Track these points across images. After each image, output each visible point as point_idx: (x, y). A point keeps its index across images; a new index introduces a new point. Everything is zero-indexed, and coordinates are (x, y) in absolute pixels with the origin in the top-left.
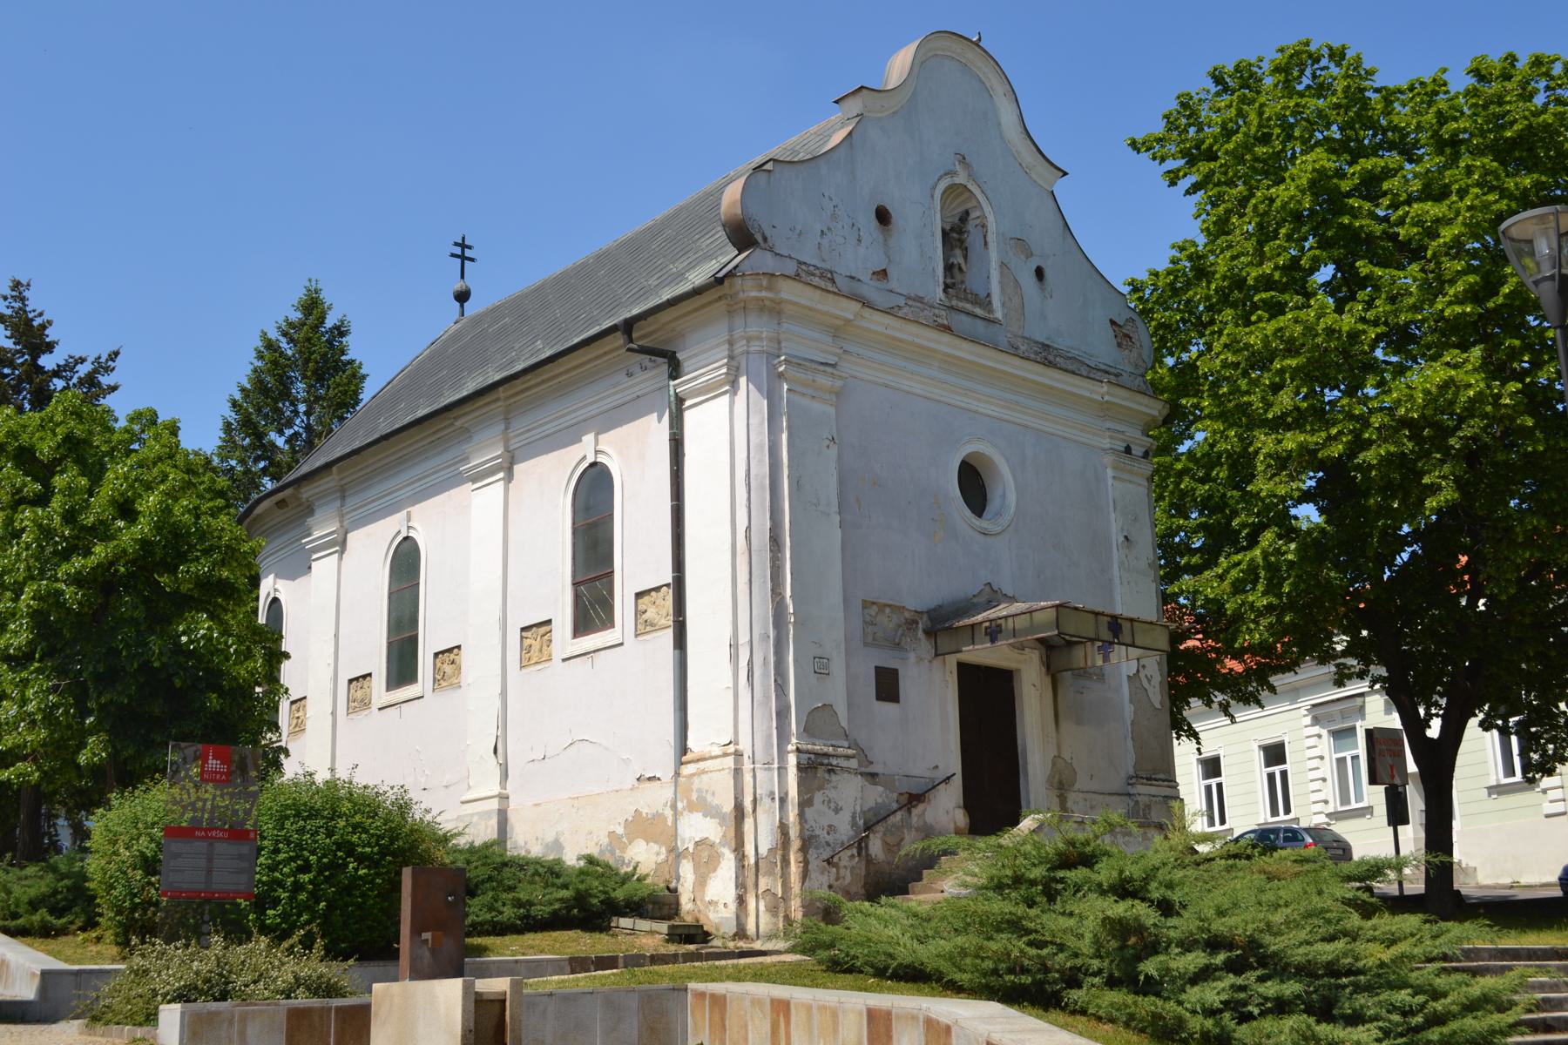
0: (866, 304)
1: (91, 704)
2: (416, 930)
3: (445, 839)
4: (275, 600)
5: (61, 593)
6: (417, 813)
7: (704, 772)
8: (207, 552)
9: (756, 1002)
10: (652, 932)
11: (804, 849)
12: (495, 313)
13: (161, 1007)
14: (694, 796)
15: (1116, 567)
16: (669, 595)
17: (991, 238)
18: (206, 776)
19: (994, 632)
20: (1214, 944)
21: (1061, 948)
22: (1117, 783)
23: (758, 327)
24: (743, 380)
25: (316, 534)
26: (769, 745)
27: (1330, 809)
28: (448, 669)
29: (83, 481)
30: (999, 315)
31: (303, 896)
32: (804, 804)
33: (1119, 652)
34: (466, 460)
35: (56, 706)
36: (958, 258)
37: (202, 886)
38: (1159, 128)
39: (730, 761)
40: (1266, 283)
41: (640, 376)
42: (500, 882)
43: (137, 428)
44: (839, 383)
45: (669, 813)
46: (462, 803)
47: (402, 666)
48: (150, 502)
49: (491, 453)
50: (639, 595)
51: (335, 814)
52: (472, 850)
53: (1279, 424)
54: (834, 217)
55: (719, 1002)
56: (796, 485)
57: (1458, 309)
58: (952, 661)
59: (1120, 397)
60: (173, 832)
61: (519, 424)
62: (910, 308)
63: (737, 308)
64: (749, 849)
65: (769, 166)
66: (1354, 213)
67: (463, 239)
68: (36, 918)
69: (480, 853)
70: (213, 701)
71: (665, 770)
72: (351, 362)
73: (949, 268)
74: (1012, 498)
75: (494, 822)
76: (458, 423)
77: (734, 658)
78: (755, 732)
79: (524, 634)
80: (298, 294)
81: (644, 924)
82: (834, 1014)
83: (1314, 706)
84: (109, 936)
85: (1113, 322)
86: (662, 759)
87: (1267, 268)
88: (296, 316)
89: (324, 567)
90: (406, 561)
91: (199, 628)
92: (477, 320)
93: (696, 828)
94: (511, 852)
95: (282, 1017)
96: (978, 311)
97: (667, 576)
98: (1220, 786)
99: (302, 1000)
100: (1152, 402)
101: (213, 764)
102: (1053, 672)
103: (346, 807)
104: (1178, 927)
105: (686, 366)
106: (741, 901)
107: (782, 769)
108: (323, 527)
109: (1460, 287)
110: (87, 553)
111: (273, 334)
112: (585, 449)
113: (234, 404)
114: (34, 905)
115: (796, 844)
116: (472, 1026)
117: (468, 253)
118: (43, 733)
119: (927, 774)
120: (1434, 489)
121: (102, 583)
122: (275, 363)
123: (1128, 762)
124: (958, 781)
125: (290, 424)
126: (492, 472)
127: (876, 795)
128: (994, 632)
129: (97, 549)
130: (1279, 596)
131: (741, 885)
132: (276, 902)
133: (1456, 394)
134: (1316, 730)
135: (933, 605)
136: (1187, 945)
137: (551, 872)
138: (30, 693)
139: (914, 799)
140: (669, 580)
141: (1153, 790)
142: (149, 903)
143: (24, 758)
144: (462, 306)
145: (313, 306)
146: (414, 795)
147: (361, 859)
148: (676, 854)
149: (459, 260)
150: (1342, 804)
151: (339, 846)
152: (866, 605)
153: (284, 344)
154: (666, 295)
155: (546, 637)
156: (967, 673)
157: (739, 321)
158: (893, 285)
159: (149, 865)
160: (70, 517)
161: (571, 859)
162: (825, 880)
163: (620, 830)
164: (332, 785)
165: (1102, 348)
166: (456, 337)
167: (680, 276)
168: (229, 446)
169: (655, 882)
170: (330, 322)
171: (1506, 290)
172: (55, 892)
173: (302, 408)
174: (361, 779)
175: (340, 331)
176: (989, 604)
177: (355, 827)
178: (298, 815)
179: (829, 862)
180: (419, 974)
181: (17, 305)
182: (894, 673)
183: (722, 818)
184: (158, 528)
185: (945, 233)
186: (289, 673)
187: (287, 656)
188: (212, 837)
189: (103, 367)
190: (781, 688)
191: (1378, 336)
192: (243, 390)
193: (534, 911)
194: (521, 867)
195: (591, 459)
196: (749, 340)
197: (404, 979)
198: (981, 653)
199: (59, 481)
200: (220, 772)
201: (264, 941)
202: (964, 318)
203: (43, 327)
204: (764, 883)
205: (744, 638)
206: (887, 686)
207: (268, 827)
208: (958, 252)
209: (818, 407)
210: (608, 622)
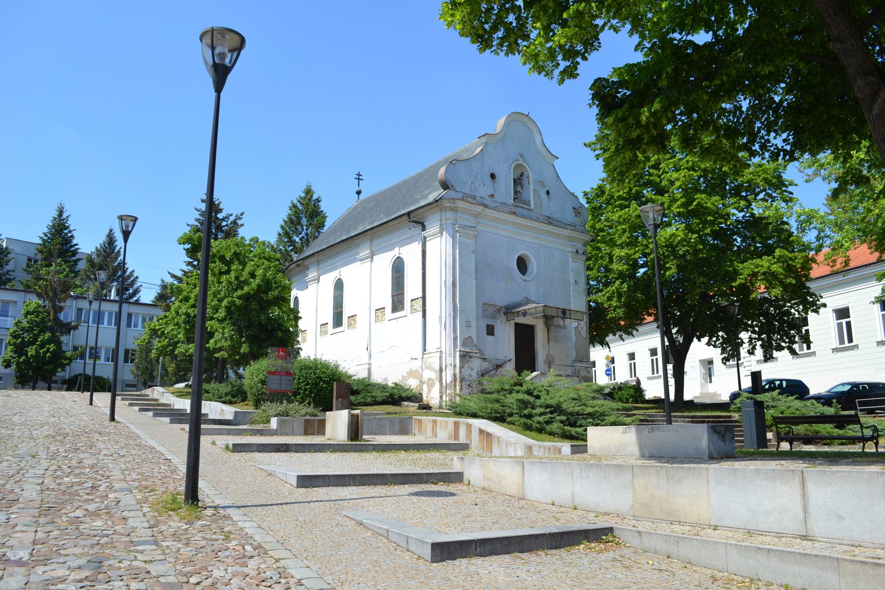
0: (485, 206)
1: (244, 335)
2: (337, 399)
3: (350, 377)
4: (296, 297)
5: (235, 301)
6: (341, 369)
8: (277, 288)
9: (429, 421)
10: (413, 406)
11: (461, 381)
12: (369, 200)
15: (571, 292)
16: (420, 302)
17: (531, 181)
18: (279, 357)
19: (525, 314)
20: (547, 406)
21: (510, 407)
22: (569, 362)
23: (450, 215)
24: (444, 232)
25: (310, 276)
26: (451, 349)
28: (353, 322)
29: (241, 267)
30: (533, 207)
31: (307, 392)
32: (461, 368)
33: (567, 321)
34: (358, 254)
35: (233, 335)
36: (519, 189)
38: (594, 139)
39: (438, 354)
40: (620, 198)
41: (413, 229)
42: (367, 390)
43: (252, 243)
44: (476, 233)
45: (420, 370)
47: (338, 320)
48: (259, 272)
49: (366, 252)
50: (412, 300)
51: (316, 369)
52: (359, 380)
53: (622, 246)
54: (476, 178)
55: (420, 421)
56: (461, 266)
57: (678, 210)
58: (513, 323)
59: (575, 234)
60: (270, 373)
61: (375, 243)
62: (501, 207)
63: (443, 209)
64: (444, 381)
65: (454, 162)
66: (650, 175)
68: (228, 398)
69: (361, 381)
70: (280, 334)
71: (419, 356)
72: (322, 211)
73: (516, 192)
74: (535, 269)
75: (366, 372)
77: (440, 321)
78: (446, 344)
80: (303, 187)
81: (411, 404)
84: (251, 403)
85: (574, 208)
86: (418, 353)
87: (621, 193)
88: (303, 195)
89: (312, 287)
90: (339, 285)
91: (275, 312)
92: (364, 201)
93: (428, 374)
94: (372, 381)
96: (525, 206)
97: (421, 295)
98: (634, 363)
99: (308, 417)
100: (586, 235)
101: (281, 353)
102: (548, 326)
103: (320, 366)
104: (538, 402)
105: (427, 227)
106: (441, 397)
107: (455, 357)
108: (312, 274)
109: (679, 203)
110: (242, 289)
111: (295, 202)
112: (395, 253)
113: (282, 227)
114: (226, 395)
115: (458, 380)
117: (361, 177)
118: (229, 343)
120: (670, 268)
121: (246, 298)
122: (296, 212)
123: (573, 355)
124: (513, 361)
125: (300, 233)
126: (366, 258)
127: (485, 365)
128: (525, 314)
129: (245, 288)
130: (621, 302)
131: (441, 392)
132: (299, 394)
133: (674, 239)
135: (507, 304)
136: (541, 406)
137: (384, 388)
138: (226, 331)
139: (498, 366)
141: (581, 365)
142: (263, 393)
143: (223, 350)
145: (309, 191)
146: (340, 363)
147: (324, 382)
148: (422, 382)
151: (318, 378)
152: (484, 304)
153: (299, 205)
154: (422, 203)
156: (518, 326)
157: (444, 213)
159: (263, 382)
160: (237, 278)
161: (390, 384)
162: (467, 391)
163: (405, 375)
164: (315, 360)
165: (570, 217)
166: (356, 207)
167: (426, 196)
168: (280, 240)
169: (416, 391)
170: (314, 197)
171: (695, 203)
172: (233, 391)
173: (305, 228)
174: (324, 358)
175: (318, 200)
176: (526, 304)
177: (322, 372)
178: (306, 368)
179: (469, 385)
180: (338, 409)
182: (493, 326)
183: (436, 371)
184: (262, 280)
185: (515, 180)
186: (301, 324)
187: (301, 318)
189: (238, 218)
190: (455, 331)
192: (284, 221)
193: (377, 399)
194: (374, 386)
195: (397, 256)
196: (446, 219)
198: (521, 320)
199: (233, 267)
201: (297, 403)
202: (521, 209)
203: (219, 204)
204: (448, 392)
205: (443, 315)
206: (490, 330)
207: (297, 372)
208: (519, 186)
209: (468, 241)
210: (402, 309)
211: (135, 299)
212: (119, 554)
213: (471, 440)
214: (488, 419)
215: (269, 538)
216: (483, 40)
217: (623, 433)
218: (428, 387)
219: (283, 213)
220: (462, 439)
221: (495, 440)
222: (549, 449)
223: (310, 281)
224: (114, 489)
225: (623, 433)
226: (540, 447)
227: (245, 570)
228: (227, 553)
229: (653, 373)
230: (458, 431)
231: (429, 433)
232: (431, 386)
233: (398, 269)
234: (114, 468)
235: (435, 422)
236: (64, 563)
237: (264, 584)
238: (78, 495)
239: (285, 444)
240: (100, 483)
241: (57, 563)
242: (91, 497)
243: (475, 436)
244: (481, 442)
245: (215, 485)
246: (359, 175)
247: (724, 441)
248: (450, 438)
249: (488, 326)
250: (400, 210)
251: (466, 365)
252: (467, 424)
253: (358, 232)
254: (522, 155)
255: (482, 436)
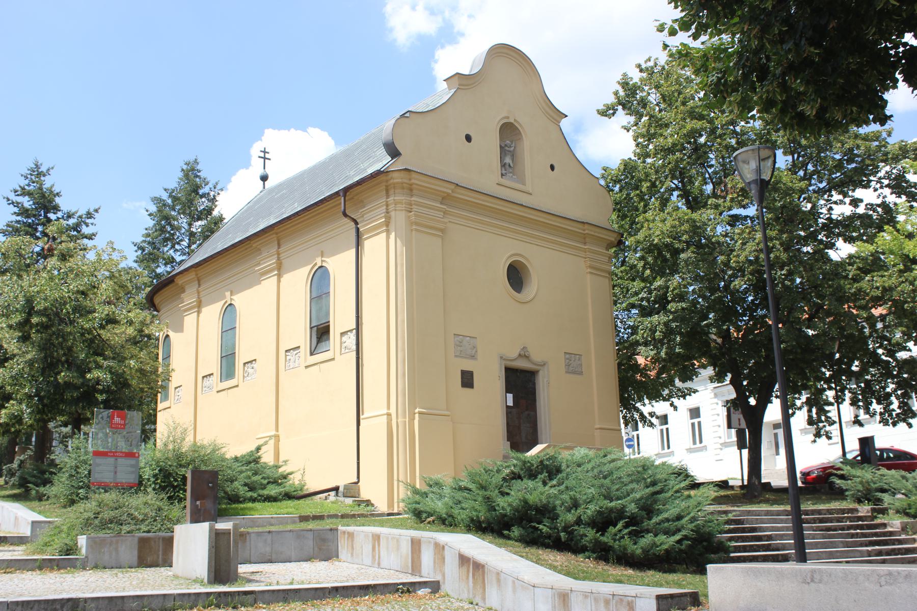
12: (280, 187)
13: (79, 537)
16: (353, 336)
27: (722, 441)
28: (250, 371)
37: (112, 480)
46: (257, 439)
55: (351, 535)
65: (407, 115)
67: (265, 148)
76: (254, 245)
79: (287, 354)
82: (398, 541)
83: (715, 388)
92: (272, 190)
95: (136, 540)
97: (354, 327)
108: (189, 298)
116: (214, 544)
117: (267, 156)
134: (716, 400)
140: (355, 327)
144: (264, 184)
149: (263, 160)
150: (728, 438)
155: (297, 355)
188: (116, 456)
191: (105, 359)
197: (185, 521)
200: (120, 424)
213: (444, 575)
214: (469, 530)
220: (428, 573)
221: (490, 578)
223: (186, 311)
229: (694, 443)
230: (419, 557)
239: (69, 600)
245: (149, 581)
246: (265, 152)
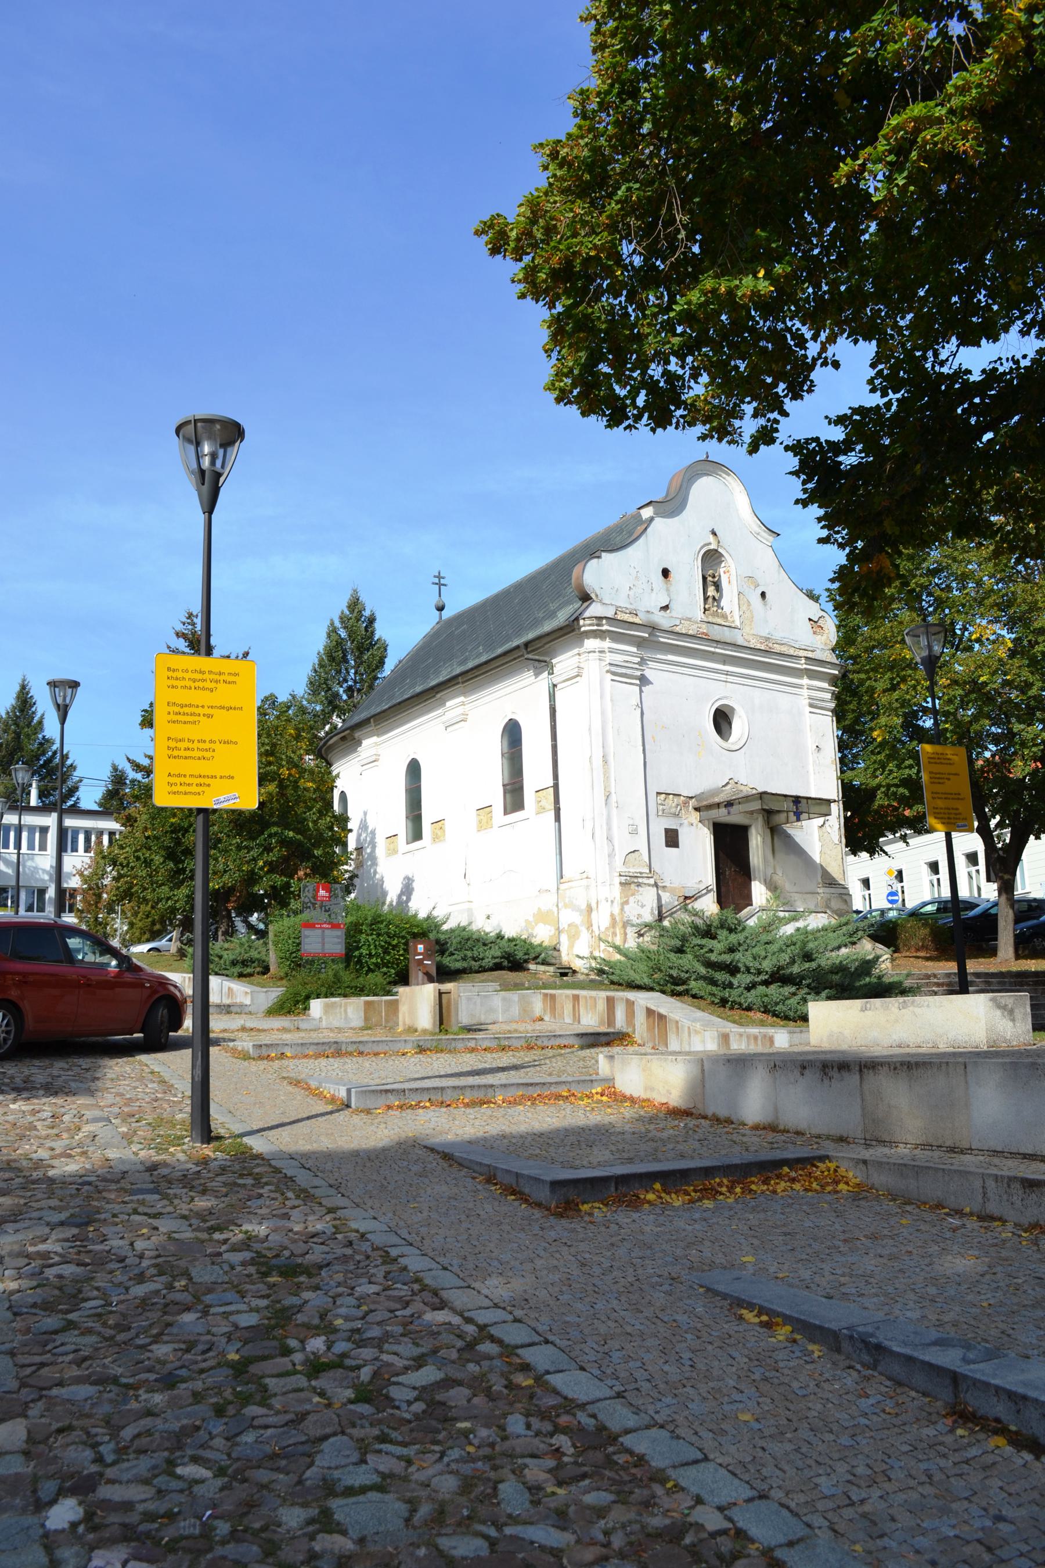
7: (571, 888)
9: (567, 996)
14: (567, 900)
28: (439, 833)
45: (555, 909)
76: (438, 696)
117: (442, 582)
119: (696, 886)
145: (355, 604)
148: (559, 931)
154: (547, 627)
158: (674, 614)
163: (531, 919)
167: (552, 615)
181: (190, 627)
206: (672, 839)
211: (70, 803)
212: (111, 1206)
215: (317, 1182)
216: (614, 422)
217: (862, 1010)
218: (569, 938)
219: (316, 643)
222: (756, 1038)
224: (85, 1118)
225: (862, 1010)
226: (741, 1035)
227: (289, 1224)
228: (260, 1202)
231: (568, 1020)
232: (574, 937)
233: (513, 733)
234: (78, 1088)
235: (576, 998)
236: (40, 1219)
237: (315, 1240)
238: (35, 1128)
240: (63, 1110)
241: (30, 1219)
242: (55, 1131)
243: (640, 1018)
244: (650, 1029)
246: (439, 577)
247: (1013, 1020)
248: (601, 1023)
249: (667, 831)
250: (509, 639)
251: (632, 899)
252: (628, 1001)
253: (441, 679)
254: (714, 533)
255: (651, 1020)
